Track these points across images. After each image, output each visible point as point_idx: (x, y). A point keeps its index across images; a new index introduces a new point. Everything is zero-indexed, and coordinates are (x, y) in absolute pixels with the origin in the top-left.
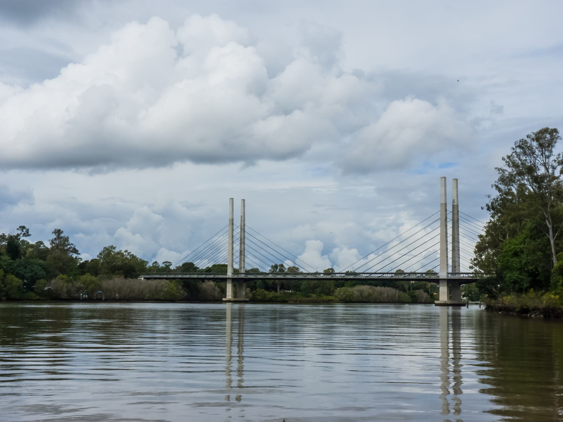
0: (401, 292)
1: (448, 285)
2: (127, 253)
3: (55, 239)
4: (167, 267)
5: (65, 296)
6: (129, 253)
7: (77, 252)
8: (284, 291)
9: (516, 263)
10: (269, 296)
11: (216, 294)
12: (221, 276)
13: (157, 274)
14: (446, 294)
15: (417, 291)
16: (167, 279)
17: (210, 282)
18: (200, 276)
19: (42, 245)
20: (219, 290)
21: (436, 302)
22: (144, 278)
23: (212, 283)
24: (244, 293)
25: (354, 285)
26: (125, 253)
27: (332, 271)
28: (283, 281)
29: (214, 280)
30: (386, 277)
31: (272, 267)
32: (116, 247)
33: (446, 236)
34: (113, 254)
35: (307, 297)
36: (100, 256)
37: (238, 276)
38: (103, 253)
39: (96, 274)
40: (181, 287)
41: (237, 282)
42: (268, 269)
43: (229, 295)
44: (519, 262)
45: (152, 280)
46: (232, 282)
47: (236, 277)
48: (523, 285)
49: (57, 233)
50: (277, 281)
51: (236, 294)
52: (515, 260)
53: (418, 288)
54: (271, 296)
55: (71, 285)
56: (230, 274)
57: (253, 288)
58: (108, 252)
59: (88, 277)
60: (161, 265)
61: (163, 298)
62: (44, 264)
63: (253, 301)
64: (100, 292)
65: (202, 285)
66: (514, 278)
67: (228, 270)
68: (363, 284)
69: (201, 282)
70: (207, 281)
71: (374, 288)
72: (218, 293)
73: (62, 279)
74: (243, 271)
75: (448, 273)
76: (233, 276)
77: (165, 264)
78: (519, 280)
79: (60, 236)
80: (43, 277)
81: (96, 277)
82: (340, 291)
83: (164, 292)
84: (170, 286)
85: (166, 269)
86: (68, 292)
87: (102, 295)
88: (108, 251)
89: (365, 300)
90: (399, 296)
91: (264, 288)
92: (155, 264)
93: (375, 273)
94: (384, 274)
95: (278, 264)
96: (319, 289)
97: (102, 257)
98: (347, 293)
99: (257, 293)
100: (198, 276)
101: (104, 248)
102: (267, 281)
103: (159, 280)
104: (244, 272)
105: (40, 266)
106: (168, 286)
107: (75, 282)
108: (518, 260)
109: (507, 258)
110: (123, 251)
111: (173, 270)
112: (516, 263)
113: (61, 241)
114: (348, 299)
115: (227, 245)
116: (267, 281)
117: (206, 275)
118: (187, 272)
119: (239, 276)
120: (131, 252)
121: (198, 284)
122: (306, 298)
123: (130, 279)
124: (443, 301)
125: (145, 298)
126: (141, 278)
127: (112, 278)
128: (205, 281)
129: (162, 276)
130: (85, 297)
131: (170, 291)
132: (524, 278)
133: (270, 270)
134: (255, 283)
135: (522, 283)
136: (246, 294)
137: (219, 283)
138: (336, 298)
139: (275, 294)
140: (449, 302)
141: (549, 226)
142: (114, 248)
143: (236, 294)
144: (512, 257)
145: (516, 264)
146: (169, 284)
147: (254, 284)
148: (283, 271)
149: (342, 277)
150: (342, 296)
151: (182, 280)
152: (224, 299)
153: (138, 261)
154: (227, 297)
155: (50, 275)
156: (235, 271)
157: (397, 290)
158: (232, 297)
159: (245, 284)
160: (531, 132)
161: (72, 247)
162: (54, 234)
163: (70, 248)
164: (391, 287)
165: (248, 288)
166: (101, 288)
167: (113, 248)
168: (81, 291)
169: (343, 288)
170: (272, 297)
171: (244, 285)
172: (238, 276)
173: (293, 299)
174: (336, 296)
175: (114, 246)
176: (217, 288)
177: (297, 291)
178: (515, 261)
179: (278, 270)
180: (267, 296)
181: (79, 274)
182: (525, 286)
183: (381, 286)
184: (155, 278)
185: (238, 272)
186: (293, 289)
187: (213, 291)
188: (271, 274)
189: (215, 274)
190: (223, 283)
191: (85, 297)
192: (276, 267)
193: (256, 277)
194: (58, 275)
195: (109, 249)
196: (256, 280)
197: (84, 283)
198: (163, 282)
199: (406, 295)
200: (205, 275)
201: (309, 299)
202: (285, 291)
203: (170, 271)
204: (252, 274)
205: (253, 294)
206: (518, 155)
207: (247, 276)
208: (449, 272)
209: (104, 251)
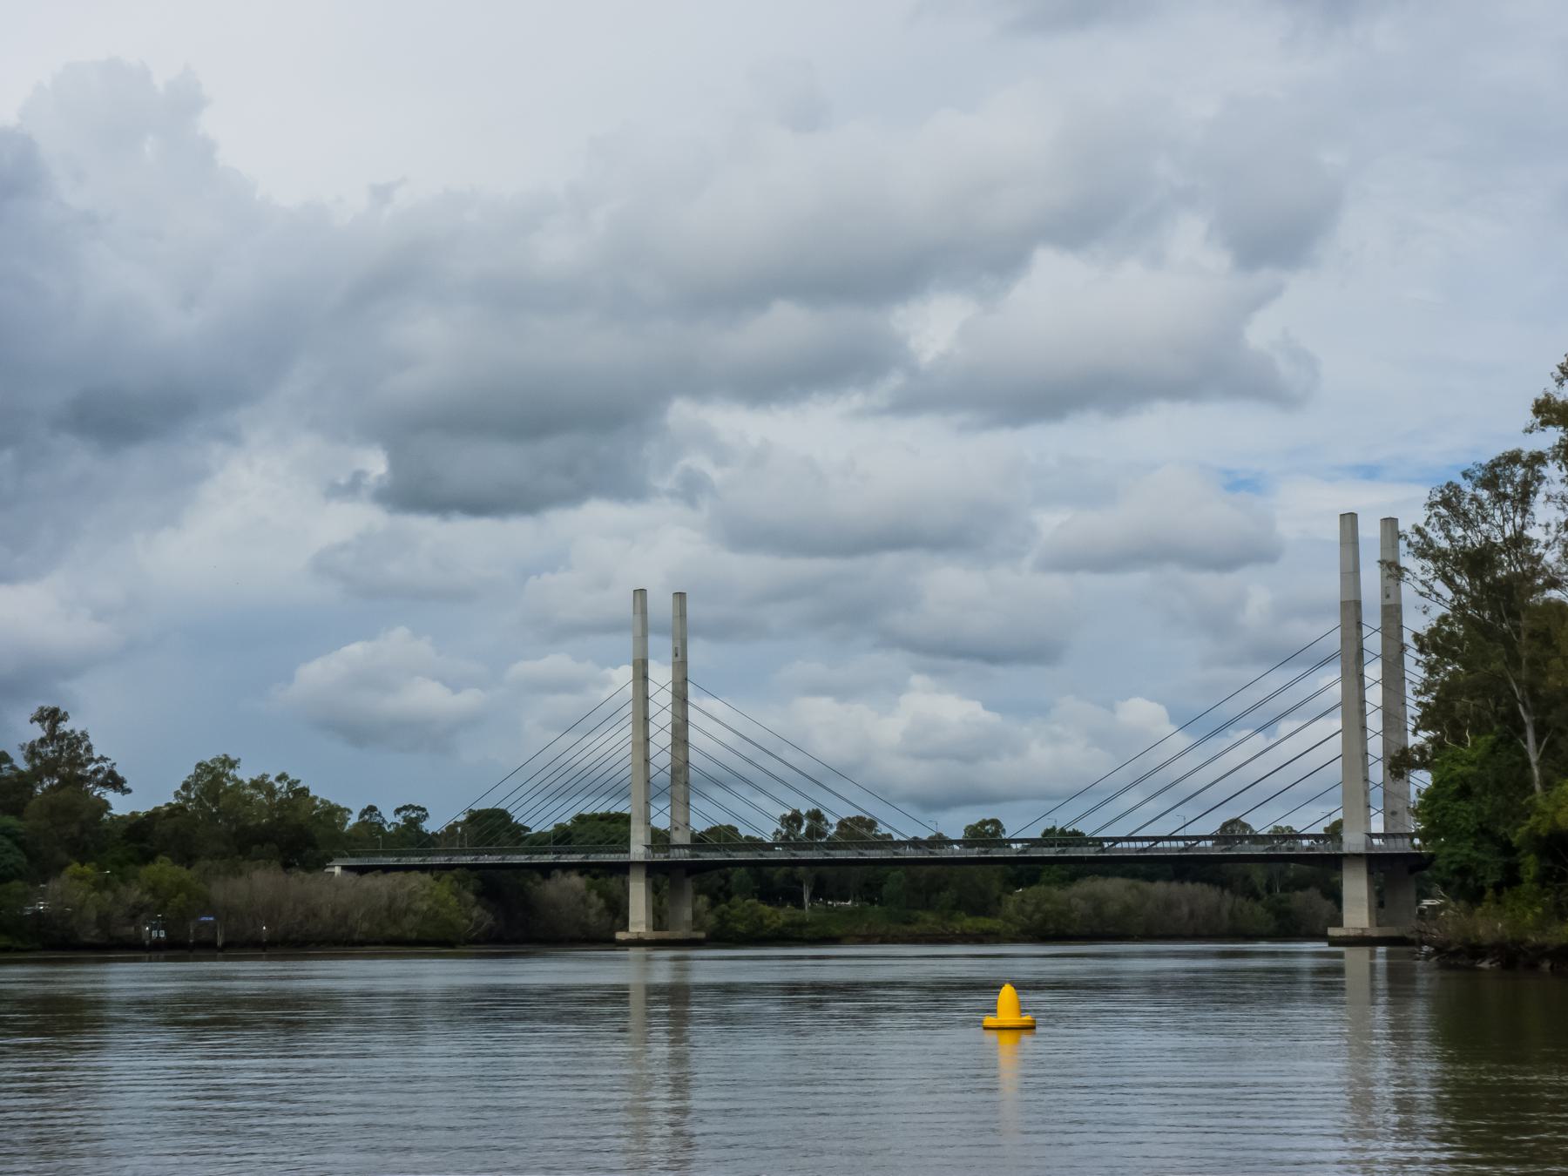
0: (1240, 900)
1: (1370, 873)
2: (286, 785)
3: (42, 741)
4: (412, 824)
5: (92, 934)
6: (291, 784)
7: (122, 787)
8: (827, 905)
9: (1465, 815)
10: (774, 922)
11: (593, 919)
12: (607, 856)
13: (385, 854)
14: (1366, 904)
15: (1299, 893)
16: (423, 868)
17: (569, 877)
18: (537, 859)
19: (7, 766)
20: (602, 903)
21: (1333, 932)
22: (344, 868)
23: (576, 881)
24: (687, 914)
25: (1073, 878)
26: (278, 785)
27: (996, 833)
28: (825, 869)
29: (583, 869)
30: (1163, 849)
31: (785, 820)
32: (239, 759)
33: (1363, 713)
34: (228, 784)
35: (908, 923)
36: (184, 793)
37: (668, 857)
38: (196, 784)
39: (187, 858)
40: (472, 897)
41: (662, 874)
42: (767, 830)
43: (639, 919)
44: (1473, 814)
45: (376, 876)
46: (648, 876)
47: (660, 857)
48: (1483, 878)
49: (47, 719)
50: (802, 869)
51: (659, 917)
52: (1461, 808)
53: (1301, 884)
54: (781, 921)
55: (110, 899)
56: (638, 850)
57: (720, 895)
58: (213, 778)
59: (164, 869)
60: (391, 819)
61: (414, 935)
62: (21, 830)
63: (722, 937)
64: (207, 919)
65: (542, 887)
66: (1458, 858)
67: (632, 834)
68: (1106, 875)
69: (538, 877)
70: (559, 873)
71: (1144, 885)
72: (599, 914)
73: (82, 878)
74: (680, 838)
75: (1372, 836)
76: (649, 857)
77: (403, 813)
78: (1474, 865)
79: (57, 733)
80: (19, 875)
81: (188, 868)
82: (1023, 901)
83: (415, 913)
84: (435, 893)
85: (411, 835)
86: (104, 920)
87: (215, 927)
88: (210, 778)
89: (1111, 929)
90: (1232, 914)
91: (756, 895)
92: (367, 817)
93: (1129, 839)
94: (1157, 842)
95: (803, 812)
96: (948, 893)
97: (193, 796)
98: (1047, 906)
99: (734, 912)
100: (530, 859)
101: (199, 765)
102: (767, 870)
103: (399, 875)
104: (689, 842)
105: (9, 836)
106: (430, 895)
107: (122, 888)
108: (1471, 808)
109: (1442, 802)
110: (272, 779)
111: (441, 834)
112: (1465, 815)
113: (62, 747)
114: (1051, 926)
115: (629, 748)
116: (767, 870)
117: (559, 853)
118: (490, 844)
119: (672, 855)
120: (298, 781)
121: (530, 884)
122: (905, 927)
123: (302, 873)
124: (1357, 929)
125: (356, 937)
126: (334, 866)
127: (241, 873)
128: (553, 873)
129: (404, 861)
130: (158, 937)
131: (437, 912)
132: (1487, 858)
133: (777, 832)
134: (727, 878)
135: (1481, 875)
136: (696, 915)
137: (601, 879)
138: (1009, 925)
139: (794, 915)
140: (1375, 933)
141: (1526, 718)
142: (233, 765)
143: (659, 917)
144: (1455, 801)
145: (1466, 819)
146: (432, 889)
147: (723, 882)
148: (822, 834)
149: (1018, 853)
150: (1030, 918)
151: (475, 873)
152: (620, 936)
153: (316, 807)
154: (631, 929)
155: (44, 869)
156: (659, 839)
157: (1226, 893)
158: (647, 927)
159: (693, 881)
160: (1473, 464)
161: (104, 768)
162: (36, 724)
163: (96, 772)
164: (1203, 881)
165: (700, 897)
166: (209, 907)
167: (227, 764)
168: (143, 916)
169: (1034, 888)
170: (786, 925)
171: (689, 885)
172: (668, 857)
173: (857, 931)
174: (1008, 919)
175: (233, 757)
176: (593, 897)
177: (872, 902)
178: (1463, 811)
179: (803, 831)
180: (766, 922)
181: (131, 860)
182: (1491, 880)
183: (1169, 879)
184: (386, 869)
185: (668, 840)
186: (858, 898)
187: (582, 906)
188: (778, 845)
189: (587, 852)
190: (614, 879)
191: (158, 937)
192: (794, 820)
193: (730, 856)
194: (68, 864)
195: (214, 768)
196: (729, 869)
197: (153, 890)
198: (415, 881)
199: (1259, 909)
200: (554, 853)
201: (914, 928)
202: (830, 903)
203: (428, 843)
204: (714, 849)
205: (719, 916)
206: (1444, 526)
207: (698, 856)
208: (1373, 832)
209: (198, 777)
